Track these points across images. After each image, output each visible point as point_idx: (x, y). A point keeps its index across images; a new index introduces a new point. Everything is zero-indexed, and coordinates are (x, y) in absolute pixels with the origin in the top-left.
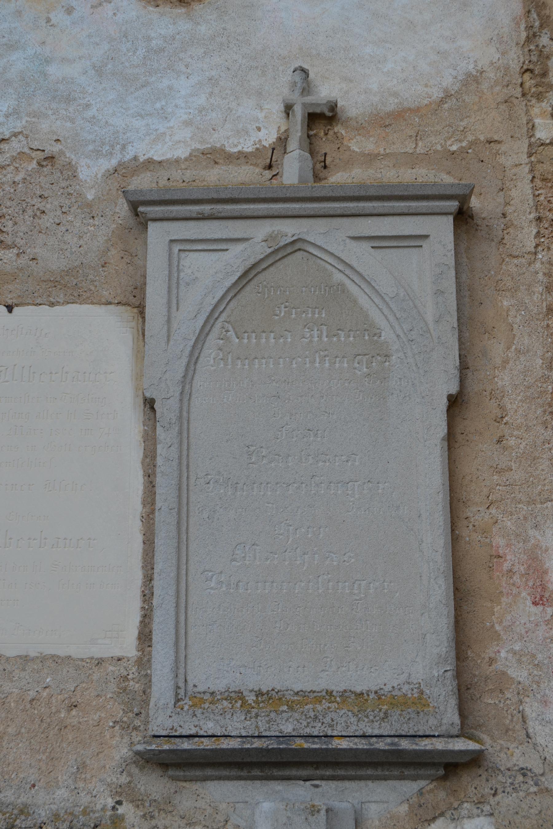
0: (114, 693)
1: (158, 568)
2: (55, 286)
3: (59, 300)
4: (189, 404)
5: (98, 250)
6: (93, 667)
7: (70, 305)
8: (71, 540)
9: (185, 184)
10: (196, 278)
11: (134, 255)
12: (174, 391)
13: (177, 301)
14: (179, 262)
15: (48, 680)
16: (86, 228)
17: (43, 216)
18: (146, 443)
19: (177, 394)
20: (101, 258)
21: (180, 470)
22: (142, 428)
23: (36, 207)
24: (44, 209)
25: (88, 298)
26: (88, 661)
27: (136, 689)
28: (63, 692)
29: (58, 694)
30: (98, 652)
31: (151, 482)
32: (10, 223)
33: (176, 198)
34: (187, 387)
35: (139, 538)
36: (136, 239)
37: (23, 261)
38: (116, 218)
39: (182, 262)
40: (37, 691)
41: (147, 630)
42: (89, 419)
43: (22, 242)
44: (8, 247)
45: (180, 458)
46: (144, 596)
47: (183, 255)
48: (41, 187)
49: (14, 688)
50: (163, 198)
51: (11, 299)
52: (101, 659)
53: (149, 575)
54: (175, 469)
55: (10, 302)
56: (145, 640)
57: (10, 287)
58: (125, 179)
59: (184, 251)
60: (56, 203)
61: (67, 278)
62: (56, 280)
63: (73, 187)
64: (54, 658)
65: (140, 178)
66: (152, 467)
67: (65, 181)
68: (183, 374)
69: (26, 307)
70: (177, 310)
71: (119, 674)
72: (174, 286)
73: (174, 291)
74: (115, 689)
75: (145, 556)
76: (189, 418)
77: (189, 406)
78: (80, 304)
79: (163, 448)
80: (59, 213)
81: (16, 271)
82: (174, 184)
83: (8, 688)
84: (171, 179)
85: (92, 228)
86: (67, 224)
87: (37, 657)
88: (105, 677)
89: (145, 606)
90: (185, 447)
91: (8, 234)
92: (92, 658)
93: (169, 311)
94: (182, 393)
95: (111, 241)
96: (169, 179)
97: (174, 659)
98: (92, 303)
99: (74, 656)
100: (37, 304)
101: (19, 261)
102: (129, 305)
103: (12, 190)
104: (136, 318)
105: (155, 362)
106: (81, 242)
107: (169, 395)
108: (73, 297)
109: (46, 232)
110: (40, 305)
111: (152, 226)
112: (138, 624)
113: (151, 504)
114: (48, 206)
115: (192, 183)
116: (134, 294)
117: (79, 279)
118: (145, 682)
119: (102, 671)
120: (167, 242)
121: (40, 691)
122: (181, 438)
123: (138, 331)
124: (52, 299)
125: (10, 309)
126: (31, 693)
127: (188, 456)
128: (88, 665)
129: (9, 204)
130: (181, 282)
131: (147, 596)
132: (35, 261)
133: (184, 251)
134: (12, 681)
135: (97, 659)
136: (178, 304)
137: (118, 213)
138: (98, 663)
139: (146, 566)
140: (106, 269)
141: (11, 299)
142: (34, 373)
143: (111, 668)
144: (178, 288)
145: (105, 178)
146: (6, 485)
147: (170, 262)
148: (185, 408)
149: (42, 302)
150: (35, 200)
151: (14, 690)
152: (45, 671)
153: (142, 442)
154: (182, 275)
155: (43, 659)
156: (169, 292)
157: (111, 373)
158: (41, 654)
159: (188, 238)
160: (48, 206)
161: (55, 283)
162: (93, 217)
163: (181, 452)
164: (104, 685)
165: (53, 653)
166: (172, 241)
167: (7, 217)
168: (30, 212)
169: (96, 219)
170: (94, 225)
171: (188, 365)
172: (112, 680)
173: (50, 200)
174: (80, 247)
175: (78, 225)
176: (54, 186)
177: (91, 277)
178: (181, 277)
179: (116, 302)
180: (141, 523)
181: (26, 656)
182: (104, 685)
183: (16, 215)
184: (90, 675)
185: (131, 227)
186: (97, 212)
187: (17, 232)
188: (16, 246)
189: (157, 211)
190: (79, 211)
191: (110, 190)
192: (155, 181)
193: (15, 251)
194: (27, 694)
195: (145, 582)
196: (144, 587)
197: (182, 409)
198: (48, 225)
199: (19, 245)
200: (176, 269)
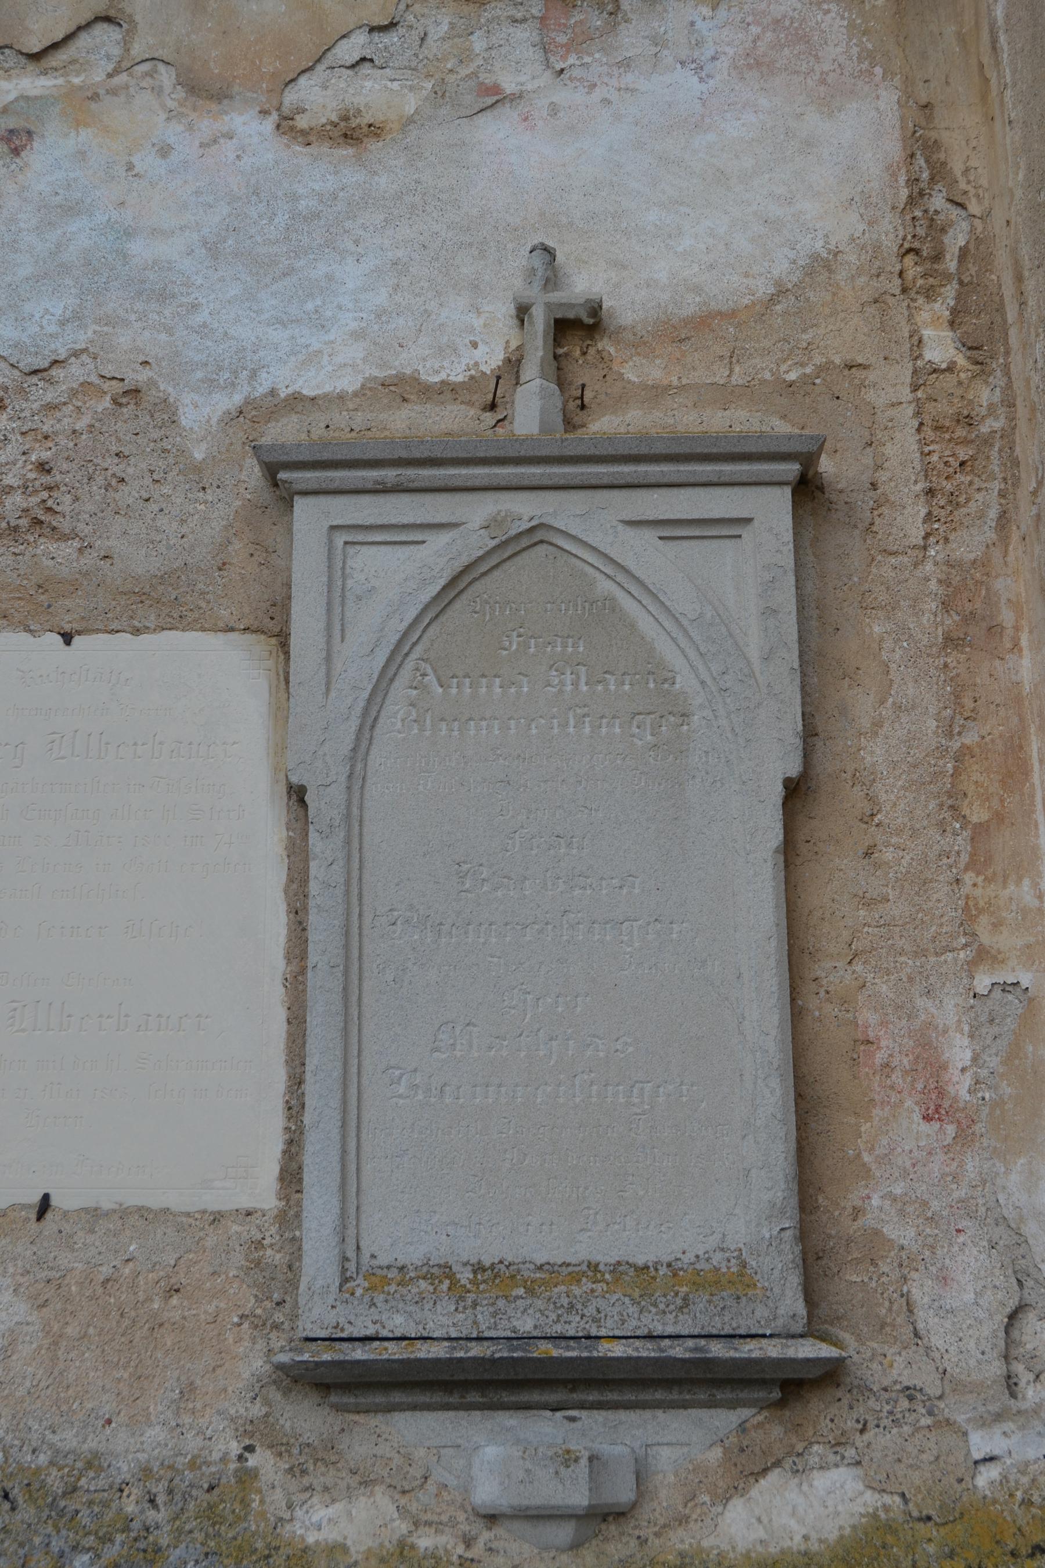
2: (142, 602)
4: (362, 794)
6: (207, 1227)
10: (374, 587)
11: (270, 550)
12: (337, 773)
13: (342, 625)
14: (344, 562)
15: (132, 1248)
17: (122, 487)
18: (292, 858)
19: (343, 779)
20: (217, 555)
21: (348, 903)
22: (284, 833)
24: (124, 475)
25: (196, 620)
26: (197, 1216)
28: (157, 1267)
30: (214, 1201)
32: (67, 499)
34: (359, 766)
35: (281, 1014)
37: (89, 560)
39: (350, 563)
41: (294, 1165)
44: (65, 538)
45: (348, 883)
46: (290, 1108)
47: (351, 550)
50: (318, 457)
51: (69, 622)
52: (219, 1212)
55: (67, 628)
57: (68, 603)
58: (256, 425)
60: (144, 466)
61: (161, 588)
64: (142, 1211)
65: (280, 425)
66: (302, 897)
68: (352, 746)
69: (95, 636)
70: (342, 641)
72: (337, 601)
73: (337, 610)
76: (361, 816)
80: (147, 481)
81: (77, 576)
82: (336, 434)
84: (331, 427)
86: (162, 499)
87: (114, 1211)
92: (204, 1212)
96: (328, 426)
98: (203, 630)
101: (82, 561)
103: (71, 445)
104: (274, 654)
106: (184, 530)
107: (329, 780)
110: (117, 632)
111: (299, 503)
112: (279, 1155)
114: (130, 470)
117: (181, 590)
122: (349, 851)
124: (136, 623)
125: (67, 638)
126: (104, 1269)
127: (360, 879)
128: (198, 1223)
129: (65, 466)
130: (348, 594)
132: (109, 561)
134: (73, 1250)
136: (343, 630)
141: (69, 622)
143: (235, 1228)
144: (343, 604)
148: (355, 801)
149: (119, 628)
150: (109, 461)
151: (76, 1265)
152: (128, 1233)
153: (285, 857)
154: (350, 583)
155: (124, 1213)
156: (329, 611)
157: (234, 743)
158: (121, 1205)
159: (360, 522)
160: (130, 470)
161: (142, 596)
162: (204, 489)
163: (349, 873)
164: (223, 1255)
165: (140, 1204)
166: (333, 528)
167: (63, 489)
168: (100, 480)
169: (208, 491)
170: (206, 502)
172: (238, 1248)
173: (133, 460)
174: (182, 537)
175: (178, 501)
177: (201, 586)
180: (284, 990)
181: (96, 1209)
182: (223, 1255)
183: (77, 485)
184: (201, 1239)
185: (265, 504)
189: (309, 479)
190: (181, 478)
191: (231, 444)
193: (76, 544)
194: (98, 1271)
198: (130, 501)
199: (82, 535)
200: (340, 573)
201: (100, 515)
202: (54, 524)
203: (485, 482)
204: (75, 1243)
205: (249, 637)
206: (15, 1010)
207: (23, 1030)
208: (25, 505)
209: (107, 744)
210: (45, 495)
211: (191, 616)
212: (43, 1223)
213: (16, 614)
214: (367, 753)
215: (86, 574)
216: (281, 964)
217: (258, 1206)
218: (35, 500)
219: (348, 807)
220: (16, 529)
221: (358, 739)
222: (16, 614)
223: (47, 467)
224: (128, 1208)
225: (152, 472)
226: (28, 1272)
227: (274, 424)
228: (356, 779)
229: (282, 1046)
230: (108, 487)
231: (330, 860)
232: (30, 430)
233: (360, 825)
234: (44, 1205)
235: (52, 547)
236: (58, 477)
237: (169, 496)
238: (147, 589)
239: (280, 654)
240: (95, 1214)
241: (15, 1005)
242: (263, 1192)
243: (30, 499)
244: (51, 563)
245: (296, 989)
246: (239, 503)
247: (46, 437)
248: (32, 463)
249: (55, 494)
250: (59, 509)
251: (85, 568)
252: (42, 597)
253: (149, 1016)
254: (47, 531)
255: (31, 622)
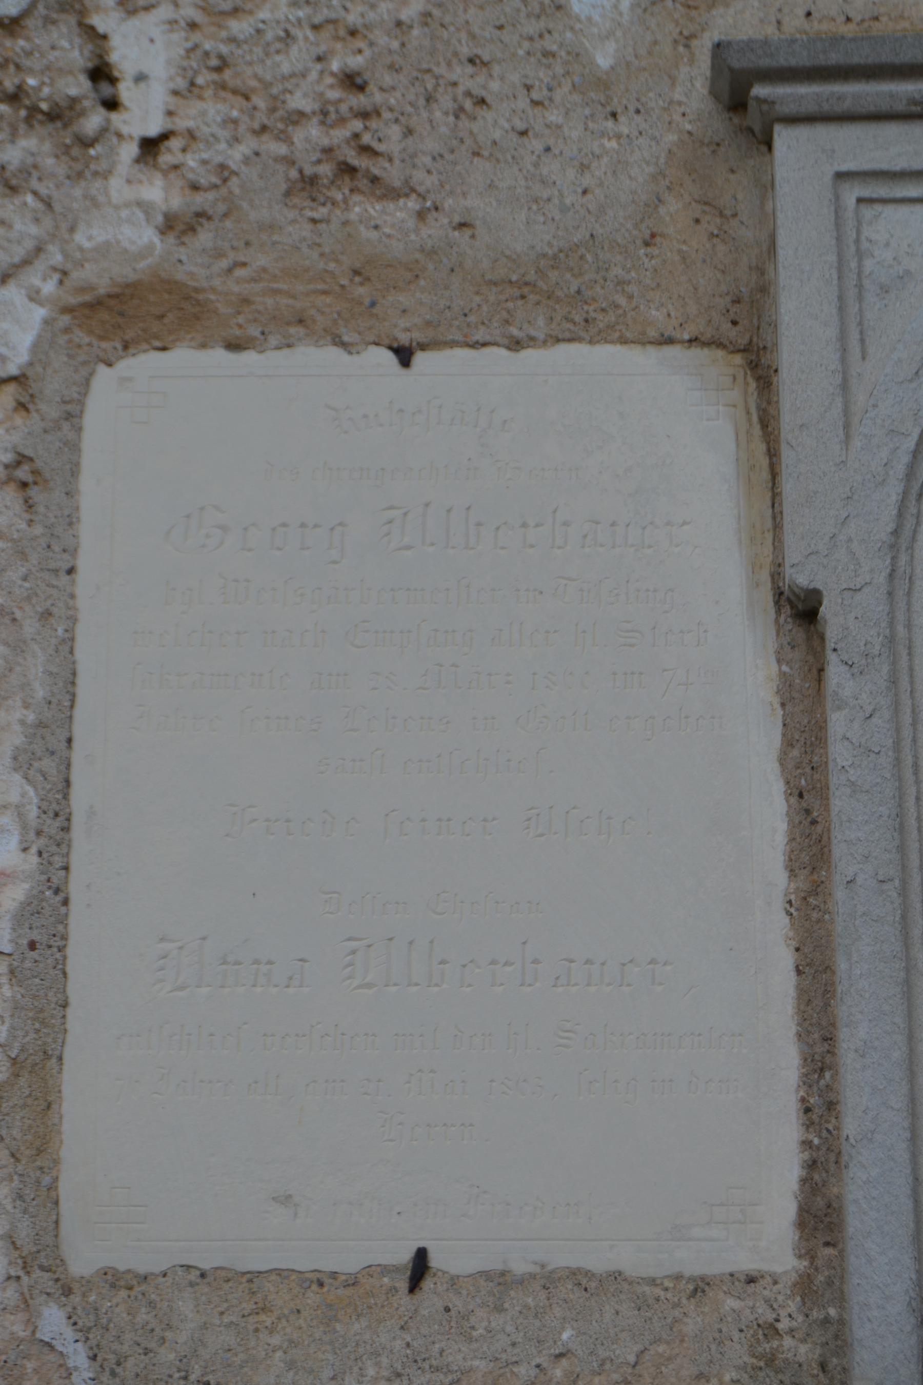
0: (743, 1368)
1: (850, 1040)
2: (523, 297)
3: (533, 333)
4: (909, 604)
5: (633, 201)
6: (684, 1301)
7: (563, 347)
8: (603, 964)
9: (852, 26)
10: (907, 272)
11: (728, 213)
12: (872, 571)
13: (861, 333)
14: (858, 232)
15: (565, 1336)
16: (596, 143)
17: (482, 112)
18: (789, 708)
19: (881, 579)
20: (642, 220)
21: (900, 779)
22: (774, 667)
23: (461, 89)
24: (483, 93)
25: (611, 327)
26: (667, 1283)
27: (801, 1359)
28: (608, 1366)
29: (595, 1373)
30: (693, 1259)
31: (808, 812)
32: (395, 132)
33: (856, 60)
34: (903, 559)
35: (784, 960)
36: (732, 171)
37: (435, 230)
38: (677, 117)
39: (866, 232)
40: (538, 1366)
41: (820, 1202)
42: (632, 645)
43: (430, 181)
44: (393, 194)
45: (897, 747)
46: (807, 1110)
47: (868, 212)
48: (472, 36)
49: (476, 1357)
50: (822, 60)
51: (407, 330)
52: (702, 1278)
53: (817, 1057)
54: (888, 776)
55: (404, 339)
56: (816, 1229)
57: (404, 299)
58: (694, 13)
59: (871, 201)
60: (515, 78)
61: (553, 275)
62: (527, 278)
63: (556, 35)
64: (579, 1277)
65: (731, 11)
66: (808, 770)
67: (533, 21)
68: (891, 527)
69: (448, 353)
70: (864, 358)
71: (752, 1318)
72: (852, 293)
73: (853, 309)
74: (746, 1359)
75: (802, 1007)
76: (910, 640)
77: (908, 610)
78: (591, 342)
79: (852, 721)
80: (523, 103)
81: (418, 256)
82: (824, 27)
83: (460, 1357)
84: (815, 14)
85: (613, 144)
86: (547, 132)
87: (533, 1276)
88: (717, 1326)
89: (811, 1137)
90: (907, 718)
91: (390, 160)
92: (678, 1277)
93: (843, 360)
94: (891, 576)
95: (664, 177)
96: (809, 14)
97: (914, 1277)
98: (623, 341)
99: (631, 1270)
100: (477, 342)
101: (425, 232)
102: (720, 345)
103: (395, 45)
104: (740, 379)
105: (815, 493)
106: (587, 181)
107: (859, 581)
108: (569, 326)
109: (491, 155)
110: (484, 345)
111: (783, 137)
112: (795, 1186)
113: (809, 868)
114: (495, 85)
115: (872, 23)
116: (732, 315)
117: (587, 277)
118: (824, 1340)
119: (706, 1309)
120: (828, 178)
121: (545, 1365)
122: (896, 695)
123: (748, 413)
124: (515, 331)
125: (404, 356)
126: (522, 1370)
127: (914, 740)
128: (669, 1295)
129: (388, 79)
130: (866, 282)
131: (820, 1108)
132: (468, 232)
133: (871, 201)
134: (470, 1340)
135: (691, 1279)
136: (862, 341)
137: (680, 103)
138: (696, 1290)
139: (809, 1032)
140: (655, 251)
141: (407, 330)
142: (479, 524)
143: (731, 1303)
144: (860, 298)
145: (639, 11)
146: (423, 820)
147: (838, 230)
148: (900, 616)
149: (488, 338)
150: (458, 70)
151: (476, 1363)
152: (557, 1311)
153: (777, 706)
154: (869, 264)
155: (547, 1279)
156: (841, 309)
157: (685, 523)
158: (543, 1266)
159: (884, 166)
160: (495, 85)
161: (524, 289)
162: (614, 115)
163: (898, 730)
164: (713, 1347)
165: (574, 1265)
166: (841, 176)
167: (386, 115)
168: (445, 101)
169: (622, 119)
170: (618, 136)
171: (902, 501)
172: (736, 1335)
173: (496, 69)
174: (585, 192)
175: (575, 134)
176: (505, 31)
177: (617, 271)
178: (867, 269)
179: (686, 337)
180: (787, 920)
181: (503, 1274)
182: (713, 1347)
183: (409, 109)
184: (676, 1321)
185: (716, 139)
186: (624, 102)
187: (414, 155)
188: (413, 190)
189: (802, 97)
190: (576, 97)
191: (656, 42)
192: (774, 20)
193: (412, 204)
194: (512, 1372)
195: (806, 1075)
196: (805, 1088)
197: (893, 618)
198: (497, 134)
199: (421, 189)
200: (853, 248)
201: (448, 157)
202: (376, 171)
203: (810, 108)
204: (473, 1328)
205: (698, 354)
206: (354, 952)
207: (369, 986)
208: (326, 142)
209: (479, 524)
210: (357, 125)
211: (603, 320)
212: (418, 1295)
213: (319, 318)
214: (914, 539)
215: (431, 253)
216: (780, 877)
217: (765, 1267)
218: (340, 135)
219: (892, 624)
220: (312, 181)
221: (900, 515)
222: (319, 318)
223: (359, 81)
224: (552, 1272)
225: (528, 88)
226: (399, 1375)
227: (721, 10)
228: (898, 582)
229: (790, 1009)
230: (459, 112)
231: (869, 709)
232: (329, 21)
233: (910, 654)
234: (420, 1267)
235: (374, 209)
236: (378, 97)
237: (559, 127)
238: (531, 276)
239: (750, 380)
240: (501, 1281)
241: (354, 944)
242: (770, 1241)
243: (332, 132)
244: (373, 235)
245: (808, 918)
246: (672, 138)
247: (353, 33)
248: (333, 74)
249: (374, 124)
250: (380, 148)
251: (430, 243)
252: (361, 290)
253: (572, 961)
254: (363, 183)
255: (343, 330)
